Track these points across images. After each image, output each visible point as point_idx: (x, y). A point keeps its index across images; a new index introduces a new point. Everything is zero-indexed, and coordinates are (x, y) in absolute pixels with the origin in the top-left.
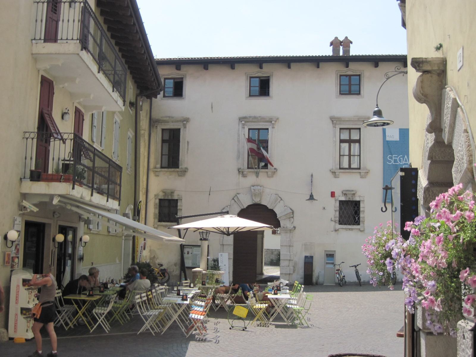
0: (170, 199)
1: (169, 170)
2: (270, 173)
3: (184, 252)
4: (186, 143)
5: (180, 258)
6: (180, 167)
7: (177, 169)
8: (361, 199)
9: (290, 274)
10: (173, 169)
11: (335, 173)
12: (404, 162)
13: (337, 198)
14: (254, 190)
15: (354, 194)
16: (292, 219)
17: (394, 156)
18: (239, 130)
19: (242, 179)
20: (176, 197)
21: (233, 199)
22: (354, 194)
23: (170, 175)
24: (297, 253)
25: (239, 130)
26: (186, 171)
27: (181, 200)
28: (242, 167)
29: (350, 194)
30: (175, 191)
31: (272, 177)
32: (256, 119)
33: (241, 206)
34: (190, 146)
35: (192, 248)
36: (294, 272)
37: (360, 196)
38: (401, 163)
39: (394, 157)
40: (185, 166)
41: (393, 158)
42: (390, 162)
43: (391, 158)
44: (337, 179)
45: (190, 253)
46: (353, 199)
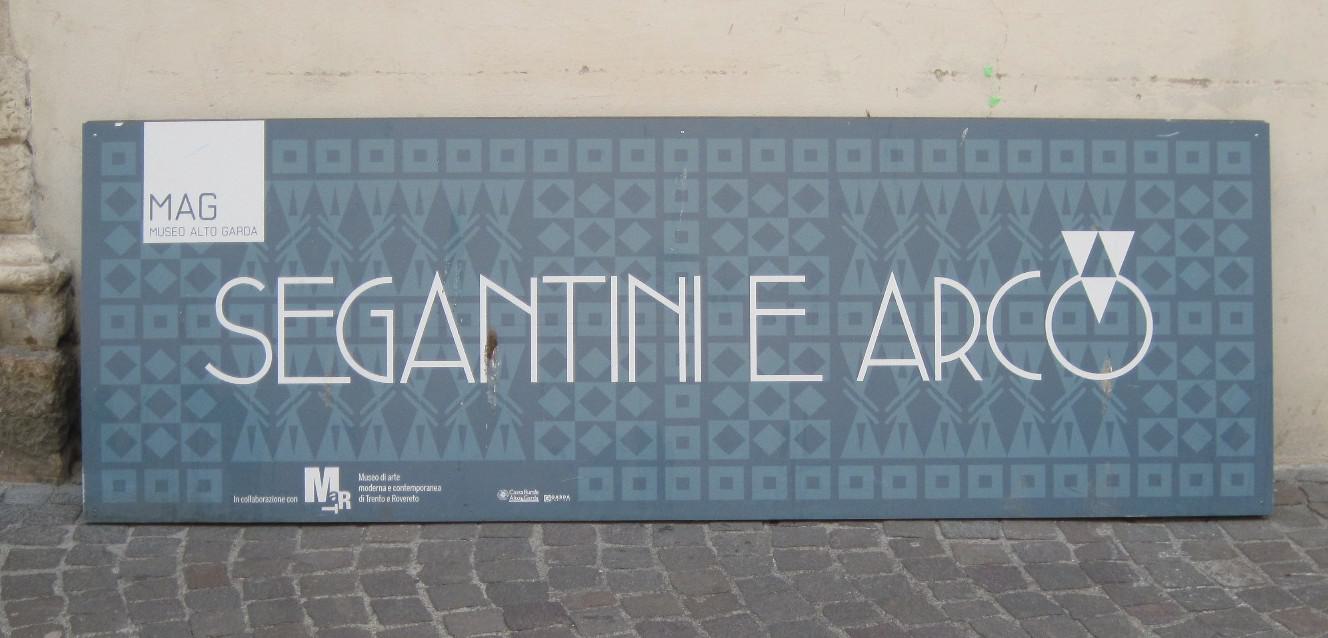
39: (295, 298)
41: (283, 314)
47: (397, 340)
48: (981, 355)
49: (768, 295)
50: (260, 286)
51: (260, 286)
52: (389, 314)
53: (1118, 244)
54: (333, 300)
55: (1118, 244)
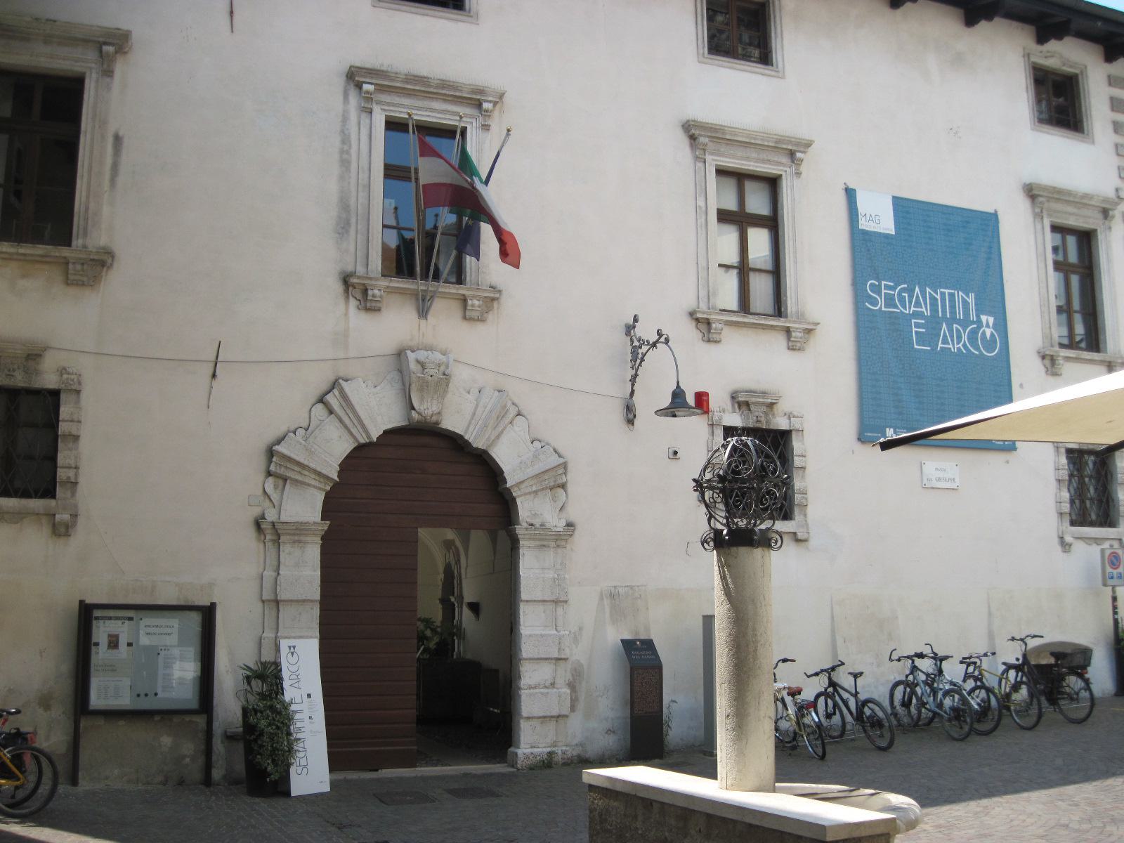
0: (21, 384)
1: (21, 251)
2: (476, 303)
3: (94, 640)
4: (110, 140)
5: (66, 667)
6: (77, 242)
7: (64, 252)
8: (796, 424)
9: (559, 716)
10: (40, 250)
11: (708, 323)
12: (912, 309)
13: (716, 418)
14: (422, 365)
15: (771, 405)
16: (560, 491)
17: (885, 285)
18: (345, 119)
19: (357, 319)
20: (49, 380)
21: (321, 400)
22: (771, 405)
23: (24, 276)
24: (581, 629)
25: (345, 119)
26: (103, 264)
27: (78, 392)
28: (361, 270)
29: (763, 404)
30: (46, 349)
31: (481, 320)
32: (417, 86)
33: (354, 431)
34: (124, 158)
35: (131, 619)
36: (573, 708)
37: (790, 416)
38: (905, 309)
39: (887, 287)
40: (103, 241)
41: (883, 291)
42: (875, 303)
43: (877, 289)
44: (712, 348)
45: (123, 641)
46: (768, 422)
47: (922, 297)
48: (964, 345)
49: (917, 325)
50: (877, 283)
51: (877, 283)
52: (906, 295)
53: (991, 320)
54: (893, 288)
55: (991, 320)
